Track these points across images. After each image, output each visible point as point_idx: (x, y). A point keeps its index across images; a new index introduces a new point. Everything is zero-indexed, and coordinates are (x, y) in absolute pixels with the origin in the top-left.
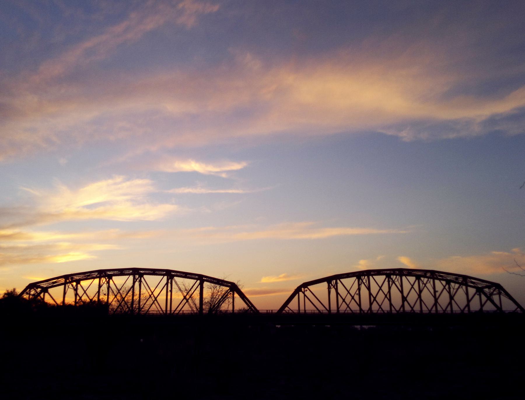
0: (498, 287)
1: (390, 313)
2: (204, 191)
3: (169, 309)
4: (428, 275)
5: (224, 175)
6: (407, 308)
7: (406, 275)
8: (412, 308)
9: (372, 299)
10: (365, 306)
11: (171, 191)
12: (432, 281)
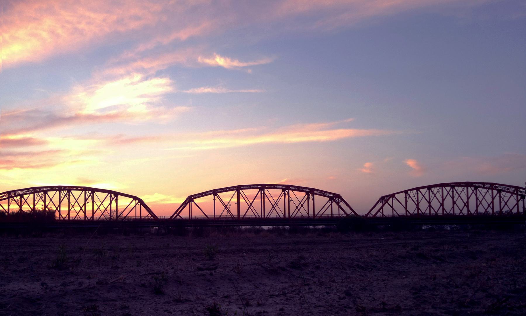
0: (338, 196)
1: (470, 215)
2: (224, 90)
3: (263, 214)
4: (13, 194)
5: (250, 71)
6: (433, 212)
7: (292, 190)
8: (461, 211)
9: (479, 203)
10: (89, 215)
11: (190, 91)
12: (466, 188)
